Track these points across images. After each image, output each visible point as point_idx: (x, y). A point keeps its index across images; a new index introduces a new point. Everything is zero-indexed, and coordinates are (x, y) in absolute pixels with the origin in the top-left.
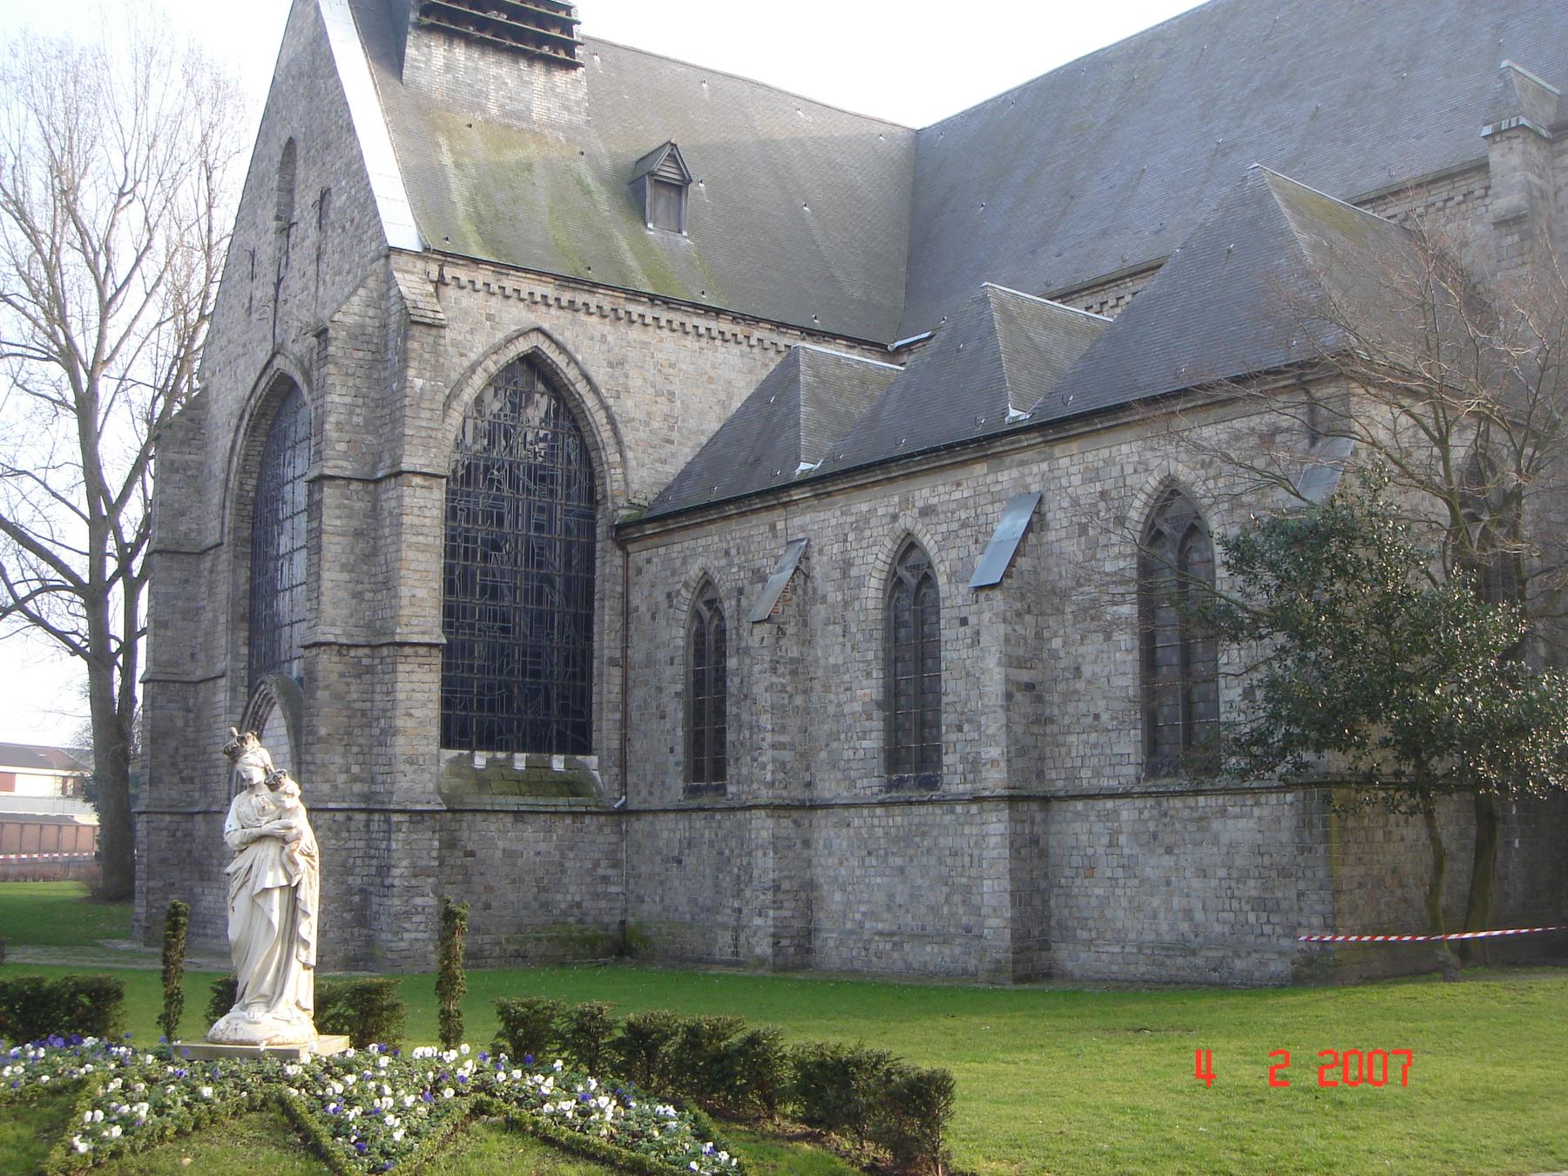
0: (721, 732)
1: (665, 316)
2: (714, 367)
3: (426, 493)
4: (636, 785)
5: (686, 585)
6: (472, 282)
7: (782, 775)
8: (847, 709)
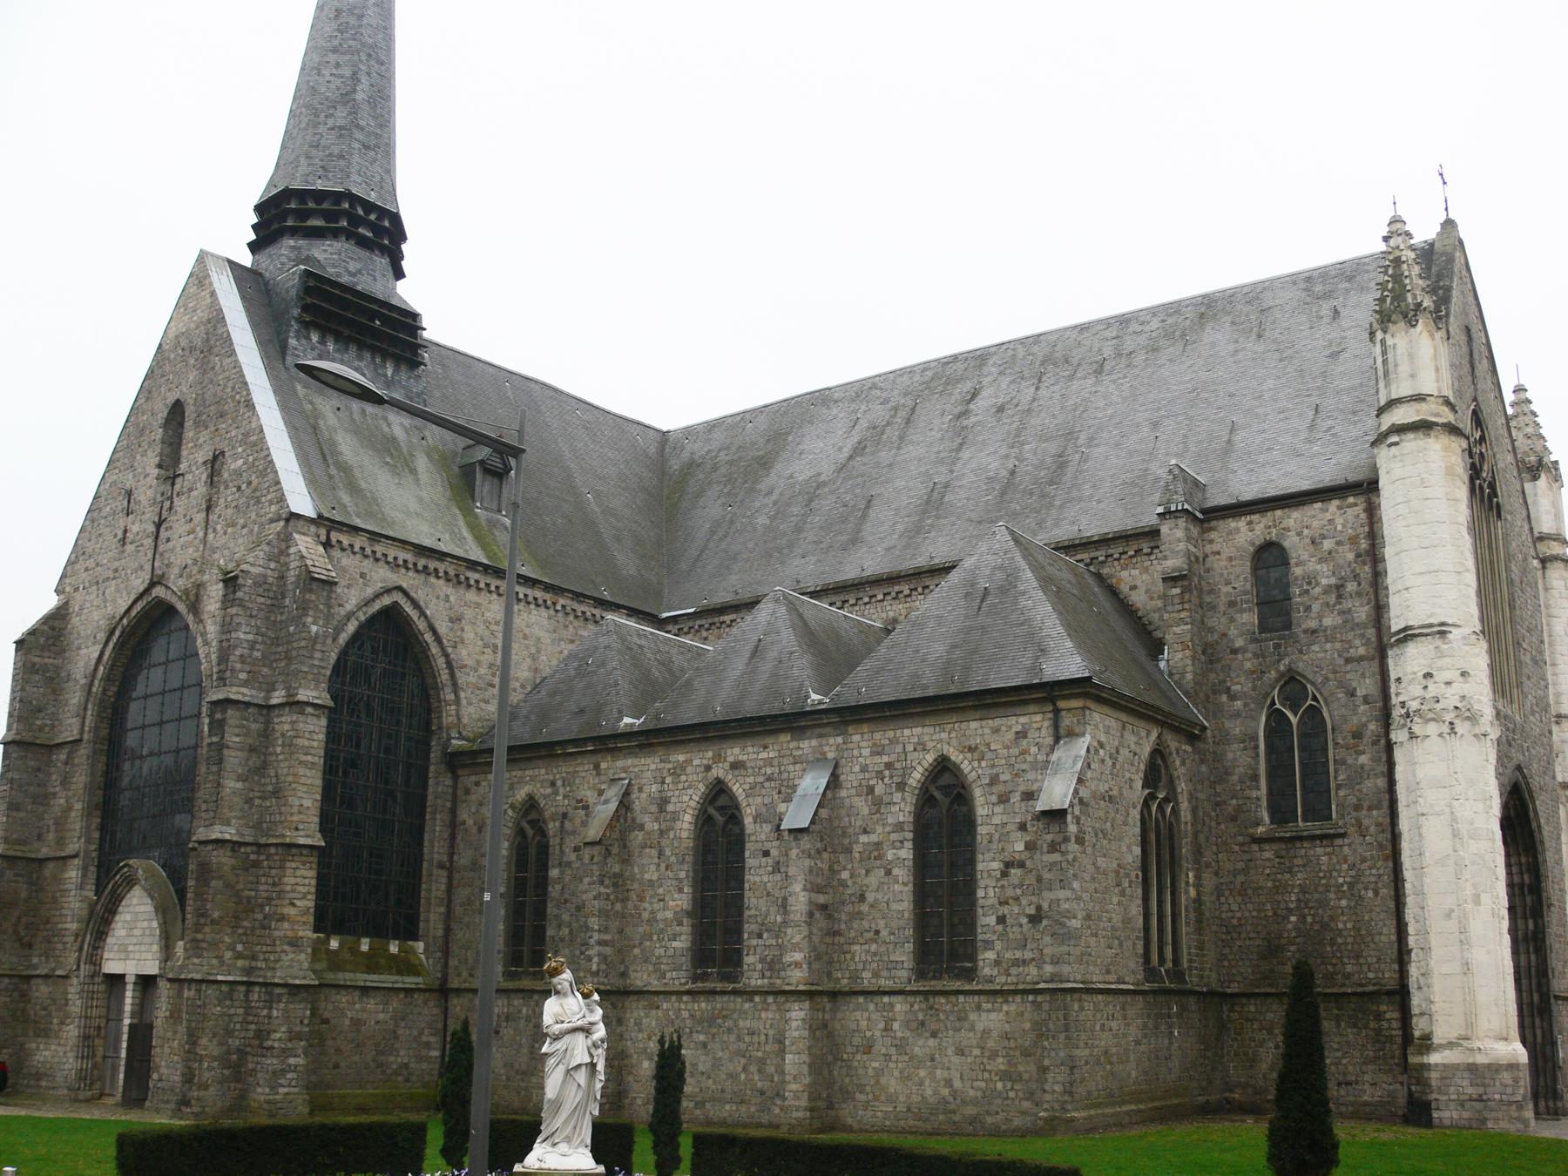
3: (315, 720)
5: (512, 806)
6: (351, 546)
8: (660, 916)
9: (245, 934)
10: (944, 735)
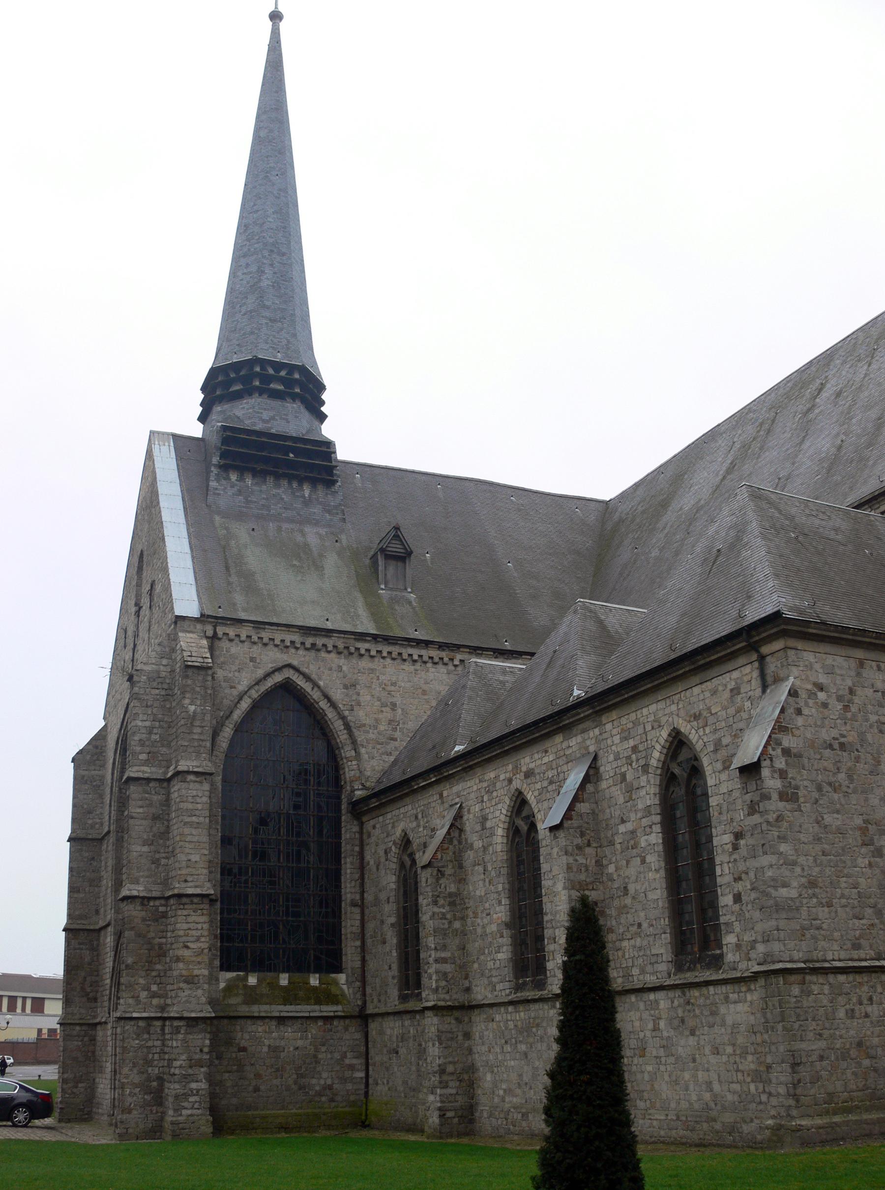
0: (418, 952)
1: (385, 649)
2: (426, 683)
3: (197, 786)
4: (371, 995)
6: (238, 636)
7: (444, 983)
9: (159, 976)
10: (674, 708)
